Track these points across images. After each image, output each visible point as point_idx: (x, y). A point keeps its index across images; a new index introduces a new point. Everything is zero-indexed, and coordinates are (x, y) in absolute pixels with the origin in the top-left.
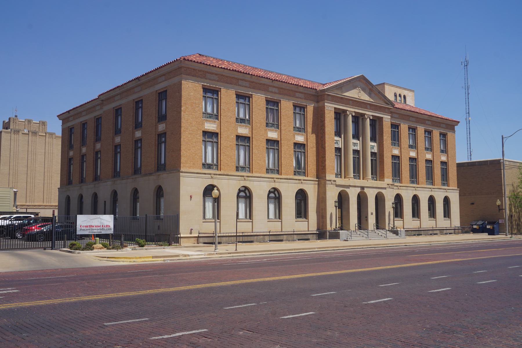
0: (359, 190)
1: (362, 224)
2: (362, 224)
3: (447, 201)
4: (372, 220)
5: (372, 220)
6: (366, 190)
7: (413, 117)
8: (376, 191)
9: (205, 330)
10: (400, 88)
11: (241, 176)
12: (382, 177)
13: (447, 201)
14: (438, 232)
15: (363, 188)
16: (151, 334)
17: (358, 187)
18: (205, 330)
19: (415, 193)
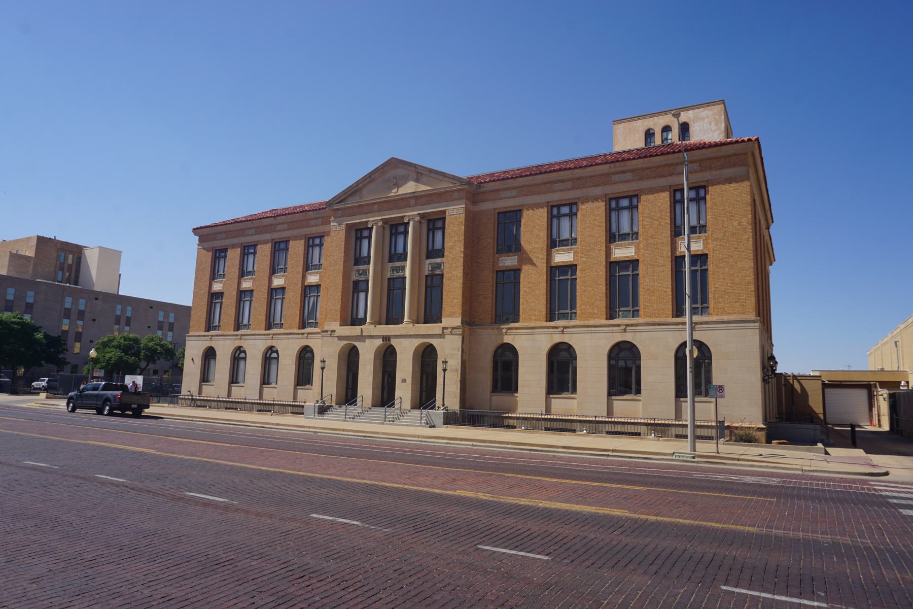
0: (379, 342)
1: (385, 397)
2: (385, 397)
3: (427, 358)
4: (404, 391)
5: (404, 391)
6: (394, 342)
7: (220, 233)
8: (417, 342)
9: (314, 515)
10: (653, 115)
11: (553, 328)
12: (398, 320)
13: (427, 358)
14: (642, 430)
15: (386, 338)
16: (547, 561)
17: (377, 337)
18: (314, 515)
19: (305, 342)
